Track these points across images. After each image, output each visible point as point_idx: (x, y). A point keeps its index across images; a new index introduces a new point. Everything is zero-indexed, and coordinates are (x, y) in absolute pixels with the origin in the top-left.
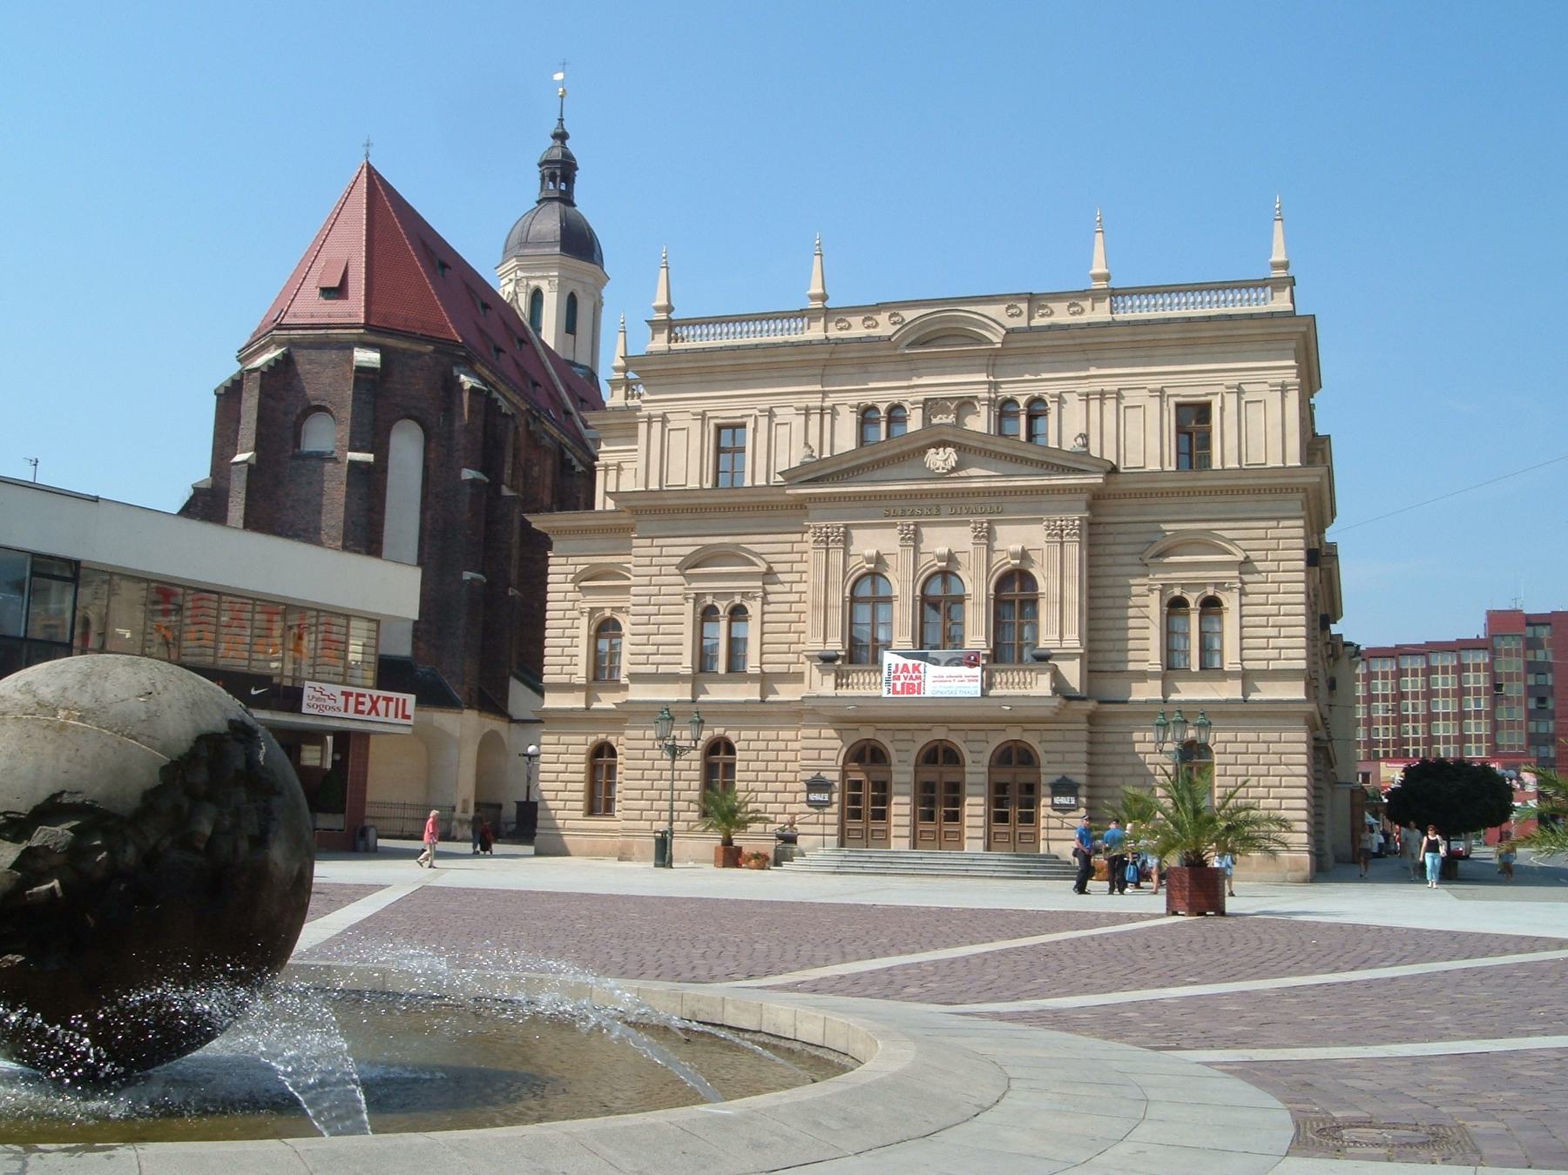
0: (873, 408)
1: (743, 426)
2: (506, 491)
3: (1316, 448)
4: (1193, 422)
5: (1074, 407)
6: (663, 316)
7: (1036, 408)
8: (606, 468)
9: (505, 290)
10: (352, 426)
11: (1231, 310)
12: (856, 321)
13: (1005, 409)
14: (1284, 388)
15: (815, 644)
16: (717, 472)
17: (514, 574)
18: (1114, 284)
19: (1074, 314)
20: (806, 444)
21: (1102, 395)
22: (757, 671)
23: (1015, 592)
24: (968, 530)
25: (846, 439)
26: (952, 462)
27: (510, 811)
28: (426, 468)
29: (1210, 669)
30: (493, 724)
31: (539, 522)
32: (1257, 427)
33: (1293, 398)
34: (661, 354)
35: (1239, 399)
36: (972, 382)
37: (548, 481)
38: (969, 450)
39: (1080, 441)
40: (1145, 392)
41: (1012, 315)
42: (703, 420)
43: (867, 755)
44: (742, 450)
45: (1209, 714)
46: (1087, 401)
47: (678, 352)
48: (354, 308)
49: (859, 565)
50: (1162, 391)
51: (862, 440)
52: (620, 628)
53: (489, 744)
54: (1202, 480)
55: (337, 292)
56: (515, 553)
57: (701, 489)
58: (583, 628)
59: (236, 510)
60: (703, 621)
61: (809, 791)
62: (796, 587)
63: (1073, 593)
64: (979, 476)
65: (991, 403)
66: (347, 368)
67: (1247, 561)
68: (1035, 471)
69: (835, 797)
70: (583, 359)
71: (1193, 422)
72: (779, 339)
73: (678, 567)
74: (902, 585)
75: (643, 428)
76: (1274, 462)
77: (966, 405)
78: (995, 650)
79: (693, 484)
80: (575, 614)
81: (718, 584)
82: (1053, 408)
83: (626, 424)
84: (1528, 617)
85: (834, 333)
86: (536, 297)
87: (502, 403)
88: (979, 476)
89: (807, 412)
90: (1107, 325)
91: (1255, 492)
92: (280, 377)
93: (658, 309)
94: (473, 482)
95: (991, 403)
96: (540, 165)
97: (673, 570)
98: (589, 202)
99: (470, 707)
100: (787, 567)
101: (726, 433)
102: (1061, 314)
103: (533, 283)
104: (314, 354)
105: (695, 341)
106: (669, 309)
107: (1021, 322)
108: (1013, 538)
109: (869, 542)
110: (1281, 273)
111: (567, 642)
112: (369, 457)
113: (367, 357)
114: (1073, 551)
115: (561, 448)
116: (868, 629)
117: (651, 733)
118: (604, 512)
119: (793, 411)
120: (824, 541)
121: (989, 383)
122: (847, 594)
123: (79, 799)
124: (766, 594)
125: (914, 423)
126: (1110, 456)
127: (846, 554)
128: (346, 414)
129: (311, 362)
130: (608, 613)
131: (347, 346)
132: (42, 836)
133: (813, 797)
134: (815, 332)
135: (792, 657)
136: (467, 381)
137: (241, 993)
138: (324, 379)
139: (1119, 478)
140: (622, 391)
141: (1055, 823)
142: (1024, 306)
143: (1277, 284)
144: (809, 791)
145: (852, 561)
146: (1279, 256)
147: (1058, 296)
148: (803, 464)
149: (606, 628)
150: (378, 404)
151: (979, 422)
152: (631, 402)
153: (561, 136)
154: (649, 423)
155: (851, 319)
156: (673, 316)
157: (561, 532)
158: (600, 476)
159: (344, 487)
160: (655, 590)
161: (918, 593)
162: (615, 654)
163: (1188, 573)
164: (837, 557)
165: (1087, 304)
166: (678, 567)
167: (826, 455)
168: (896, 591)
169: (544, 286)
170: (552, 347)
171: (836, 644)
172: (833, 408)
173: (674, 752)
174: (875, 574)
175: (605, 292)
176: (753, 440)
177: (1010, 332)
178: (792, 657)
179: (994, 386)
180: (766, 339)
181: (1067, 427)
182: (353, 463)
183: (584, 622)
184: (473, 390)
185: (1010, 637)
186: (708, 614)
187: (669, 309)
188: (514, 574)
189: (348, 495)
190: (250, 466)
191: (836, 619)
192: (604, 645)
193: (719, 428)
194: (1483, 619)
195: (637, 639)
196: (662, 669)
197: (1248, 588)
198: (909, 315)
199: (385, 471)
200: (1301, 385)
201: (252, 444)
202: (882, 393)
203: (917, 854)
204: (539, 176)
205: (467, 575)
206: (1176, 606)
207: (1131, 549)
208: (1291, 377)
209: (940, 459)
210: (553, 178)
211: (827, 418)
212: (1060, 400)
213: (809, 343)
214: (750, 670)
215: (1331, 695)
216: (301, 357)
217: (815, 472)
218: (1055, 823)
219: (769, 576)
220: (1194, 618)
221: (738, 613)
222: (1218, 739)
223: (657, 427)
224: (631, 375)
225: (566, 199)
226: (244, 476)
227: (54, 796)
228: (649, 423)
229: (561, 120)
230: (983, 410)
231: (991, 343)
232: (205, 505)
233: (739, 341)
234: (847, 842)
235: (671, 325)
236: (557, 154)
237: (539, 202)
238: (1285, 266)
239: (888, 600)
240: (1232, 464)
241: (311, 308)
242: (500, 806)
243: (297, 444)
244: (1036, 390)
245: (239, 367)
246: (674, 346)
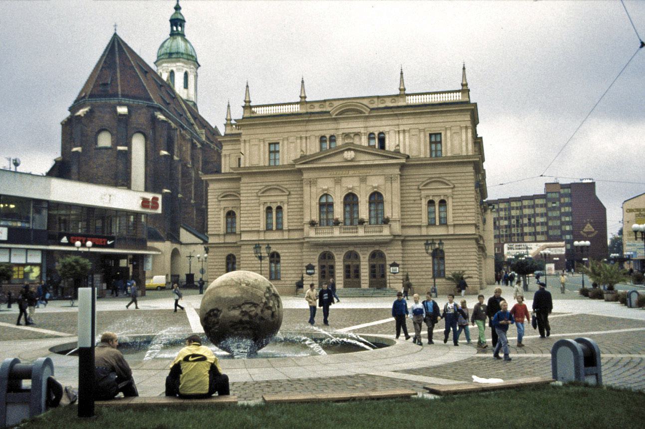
0: (324, 137)
2: (176, 158)
3: (478, 142)
4: (435, 139)
12: (317, 105)
14: (466, 128)
16: (270, 160)
21: (404, 131)
23: (376, 199)
25: (313, 147)
27: (183, 278)
33: (470, 131)
37: (189, 152)
38: (358, 150)
43: (326, 257)
45: (441, 239)
53: (175, 253)
57: (420, 294)
58: (222, 214)
64: (364, 159)
68: (383, 158)
70: (193, 98)
71: (435, 139)
88: (364, 159)
91: (459, 162)
94: (165, 156)
99: (168, 240)
108: (376, 181)
124: (288, 202)
125: (340, 142)
126: (407, 153)
133: (308, 271)
141: (391, 277)
149: (231, 215)
158: (223, 159)
166: (257, 193)
173: (261, 258)
188: (180, 190)
202: (327, 129)
203: (346, 289)
207: (414, 184)
208: (469, 124)
209: (349, 155)
215: (484, 225)
218: (391, 277)
222: (447, 247)
231: (365, 113)
242: (178, 276)
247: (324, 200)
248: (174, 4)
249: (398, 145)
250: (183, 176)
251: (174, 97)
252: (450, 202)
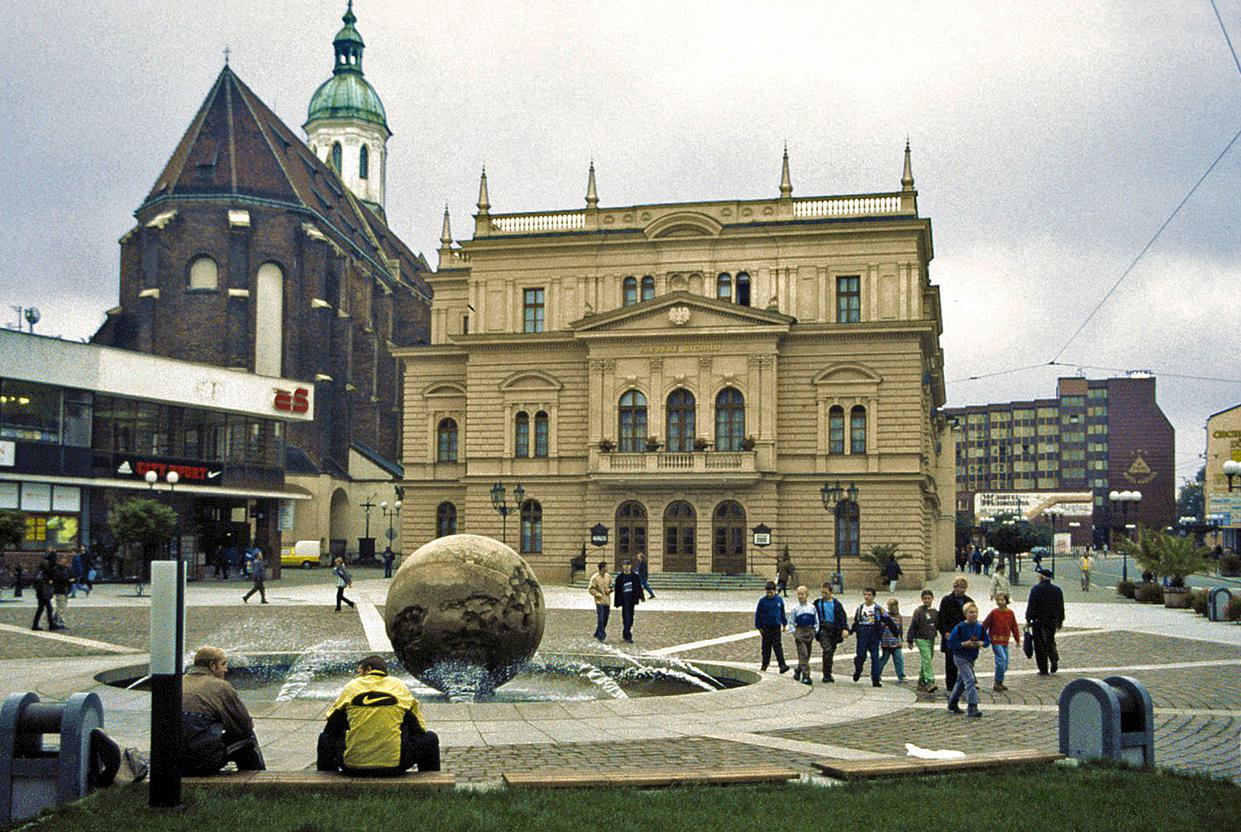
1: (542, 289)
4: (848, 287)
13: (722, 280)
14: (909, 266)
23: (730, 401)
25: (611, 299)
27: (354, 545)
28: (285, 299)
30: (340, 484)
37: (368, 303)
43: (631, 512)
45: (854, 483)
52: (456, 426)
53: (339, 498)
58: (432, 425)
61: (593, 535)
64: (708, 324)
69: (611, 539)
70: (377, 198)
71: (848, 287)
84: (1090, 382)
88: (708, 324)
91: (893, 333)
94: (322, 308)
108: (730, 368)
125: (662, 289)
133: (595, 539)
141: (755, 553)
144: (593, 535)
149: (447, 426)
153: (349, 19)
173: (504, 511)
188: (349, 376)
194: (1056, 384)
199: (255, 301)
203: (668, 574)
208: (914, 259)
209: (680, 315)
215: (937, 456)
217: (591, 320)
222: (863, 497)
231: (712, 234)
234: (539, 549)
242: (345, 542)
243: (188, 283)
247: (628, 402)
250: (355, 349)
251: (340, 194)
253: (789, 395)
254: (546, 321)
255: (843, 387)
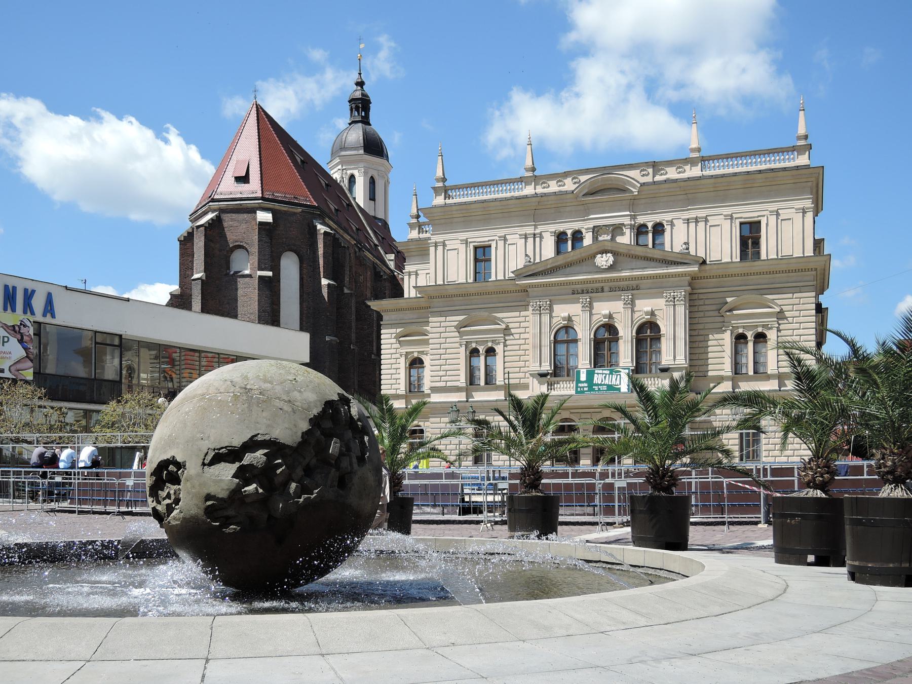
0: (564, 233)
2: (346, 291)
5: (680, 226)
6: (440, 184)
7: (659, 229)
8: (410, 274)
9: (336, 175)
10: (259, 255)
11: (773, 166)
13: (640, 230)
15: (535, 367)
16: (476, 273)
17: (353, 336)
18: (704, 153)
19: (680, 173)
20: (526, 255)
21: (697, 220)
22: (502, 383)
23: (647, 334)
24: (580, 305)
25: (548, 250)
26: (611, 262)
28: (301, 279)
29: (759, 373)
31: (374, 305)
32: (788, 233)
34: (441, 207)
35: (777, 219)
36: (622, 217)
37: (369, 285)
39: (684, 246)
40: (722, 217)
41: (643, 175)
42: (466, 243)
44: (490, 260)
46: (688, 223)
47: (451, 205)
48: (254, 187)
49: (558, 322)
50: (731, 216)
51: (558, 252)
54: (755, 266)
55: (243, 179)
56: (353, 324)
57: (467, 283)
58: (402, 364)
59: (197, 303)
60: (470, 357)
62: (522, 336)
63: (681, 333)
65: (632, 227)
66: (254, 223)
67: (782, 312)
70: (380, 215)
71: (750, 238)
72: (508, 195)
73: (455, 327)
74: (584, 334)
75: (432, 249)
76: (798, 254)
77: (617, 229)
78: (637, 366)
79: (462, 280)
80: (398, 356)
81: (481, 335)
82: (668, 228)
83: (422, 250)
85: (540, 190)
86: (352, 179)
87: (341, 240)
89: (526, 237)
90: (699, 178)
92: (215, 230)
93: (438, 180)
95: (632, 227)
96: (349, 102)
97: (453, 329)
98: (379, 123)
100: (517, 325)
101: (480, 251)
102: (672, 173)
103: (349, 172)
104: (234, 216)
105: (458, 198)
106: (444, 180)
107: (649, 179)
108: (644, 306)
109: (562, 311)
110: (802, 143)
111: (394, 371)
112: (270, 274)
113: (265, 217)
114: (681, 310)
115: (374, 266)
116: (565, 358)
117: (447, 420)
118: (409, 298)
119: (518, 236)
120: (539, 310)
121: (630, 215)
122: (552, 338)
123: (267, 438)
125: (588, 240)
126: (701, 254)
127: (551, 317)
128: (255, 249)
129: (232, 220)
130: (416, 355)
131: (252, 211)
132: (248, 458)
134: (529, 190)
135: (522, 375)
136: (321, 228)
137: (386, 524)
138: (240, 230)
139: (707, 267)
140: (417, 230)
142: (650, 170)
143: (800, 150)
145: (554, 320)
146: (802, 131)
147: (670, 163)
148: (525, 266)
149: (416, 363)
150: (273, 242)
151: (626, 238)
152: (421, 236)
153: (360, 84)
154: (436, 246)
155: (550, 183)
156: (447, 184)
157: (386, 311)
159: (257, 291)
160: (443, 340)
161: (592, 336)
162: (420, 379)
163: (747, 318)
164: (546, 318)
165: (687, 167)
166: (455, 327)
167: (538, 260)
168: (580, 336)
169: (356, 173)
170: (362, 206)
171: (547, 367)
172: (541, 234)
174: (568, 328)
175: (390, 175)
176: (496, 254)
177: (643, 185)
178: (522, 375)
179: (633, 217)
180: (501, 195)
181: (676, 239)
182: (261, 278)
183: (403, 360)
184: (325, 233)
185: (645, 360)
186: (474, 352)
187: (444, 180)
188: (353, 336)
189: (259, 295)
190: (202, 281)
191: (546, 352)
192: (414, 372)
193: (476, 248)
195: (434, 368)
196: (449, 384)
197: (782, 327)
198: (583, 178)
200: (813, 208)
201: (203, 268)
204: (349, 108)
205: (327, 338)
206: (740, 338)
208: (808, 204)
210: (357, 109)
211: (538, 240)
212: (672, 224)
213: (526, 197)
214: (498, 383)
216: (226, 217)
217: (532, 271)
219: (507, 331)
220: (750, 345)
221: (491, 352)
223: (440, 248)
224: (422, 219)
225: (366, 121)
226: (200, 287)
227: (253, 436)
228: (436, 246)
229: (360, 74)
230: (627, 231)
231: (632, 192)
232: (180, 301)
233: (485, 197)
235: (446, 191)
236: (358, 94)
237: (350, 124)
238: (806, 137)
239: (576, 341)
240: (773, 256)
241: (228, 188)
244: (658, 218)
245: (190, 224)
246: (448, 201)
247: (562, 336)
248: (355, 77)
249: (687, 243)
250: (357, 320)
251: (349, 207)
252: (499, 349)
253: (701, 326)
254: (533, 548)
255: (580, 521)
